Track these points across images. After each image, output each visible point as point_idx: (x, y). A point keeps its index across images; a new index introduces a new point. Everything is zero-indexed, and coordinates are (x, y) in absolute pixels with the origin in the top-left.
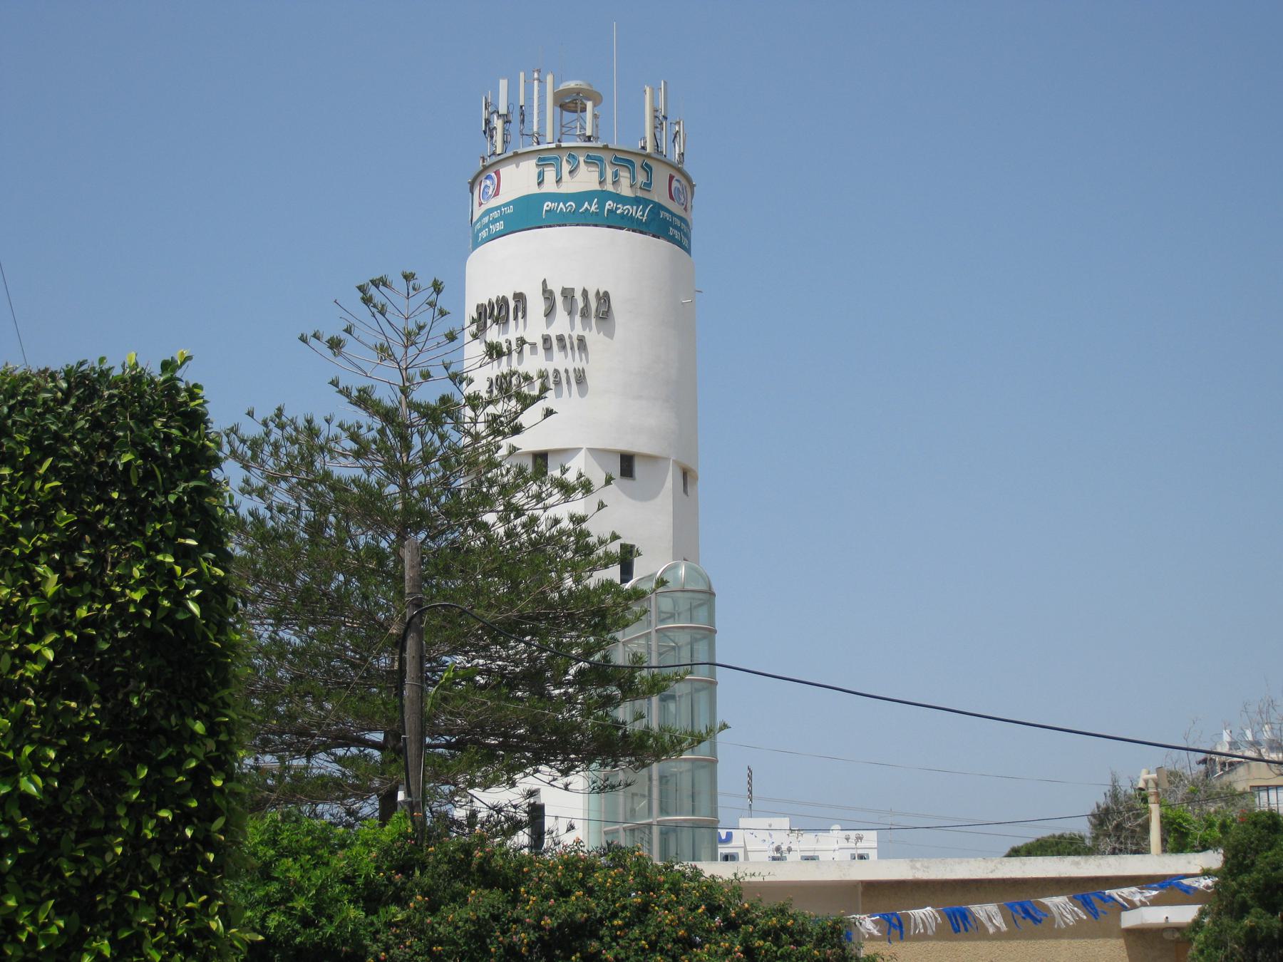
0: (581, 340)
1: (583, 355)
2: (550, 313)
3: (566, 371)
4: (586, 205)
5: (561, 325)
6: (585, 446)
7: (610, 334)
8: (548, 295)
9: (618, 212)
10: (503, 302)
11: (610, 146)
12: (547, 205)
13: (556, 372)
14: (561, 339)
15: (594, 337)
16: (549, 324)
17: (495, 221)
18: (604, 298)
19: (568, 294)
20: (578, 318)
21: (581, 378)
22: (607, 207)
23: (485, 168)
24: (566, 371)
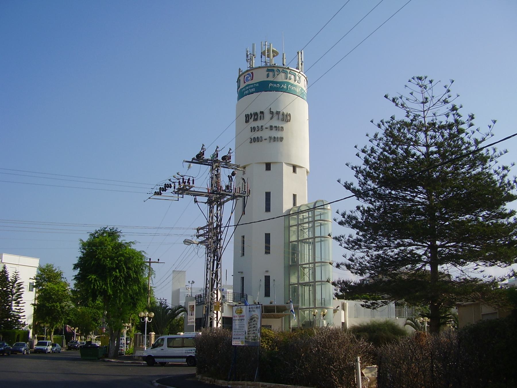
17: (251, 88)
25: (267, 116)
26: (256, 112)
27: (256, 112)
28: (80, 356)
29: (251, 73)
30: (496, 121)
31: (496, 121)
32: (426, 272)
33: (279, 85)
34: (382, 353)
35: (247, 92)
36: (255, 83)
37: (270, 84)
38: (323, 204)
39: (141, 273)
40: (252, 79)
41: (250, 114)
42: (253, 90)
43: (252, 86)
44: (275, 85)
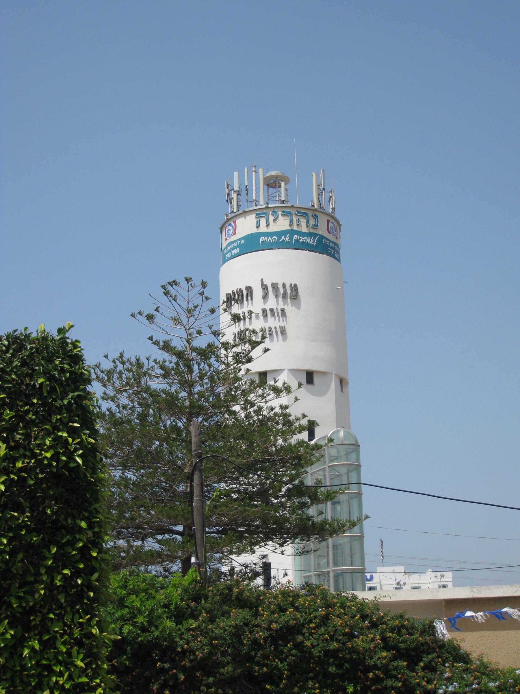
0: (283, 310)
1: (284, 318)
2: (265, 297)
3: (275, 328)
4: (283, 238)
5: (272, 303)
6: (287, 368)
7: (298, 307)
8: (264, 287)
9: (301, 241)
10: (240, 292)
11: (295, 206)
12: (262, 239)
13: (270, 328)
14: (272, 310)
15: (289, 308)
16: (265, 303)
17: (234, 248)
18: (294, 288)
19: (275, 286)
20: (280, 299)
21: (283, 331)
22: (294, 238)
23: (228, 220)
24: (275, 328)
25: (258, 293)
26: (240, 289)
27: (240, 289)
28: (326, 507)
29: (233, 222)
30: (369, 518)
31: (369, 518)
32: (315, 524)
33: (275, 237)
34: (223, 410)
35: (228, 255)
36: (239, 240)
37: (262, 239)
38: (347, 483)
39: (160, 423)
40: (235, 233)
41: (231, 292)
42: (237, 251)
43: (234, 245)
44: (270, 238)
